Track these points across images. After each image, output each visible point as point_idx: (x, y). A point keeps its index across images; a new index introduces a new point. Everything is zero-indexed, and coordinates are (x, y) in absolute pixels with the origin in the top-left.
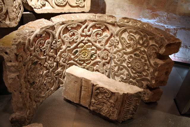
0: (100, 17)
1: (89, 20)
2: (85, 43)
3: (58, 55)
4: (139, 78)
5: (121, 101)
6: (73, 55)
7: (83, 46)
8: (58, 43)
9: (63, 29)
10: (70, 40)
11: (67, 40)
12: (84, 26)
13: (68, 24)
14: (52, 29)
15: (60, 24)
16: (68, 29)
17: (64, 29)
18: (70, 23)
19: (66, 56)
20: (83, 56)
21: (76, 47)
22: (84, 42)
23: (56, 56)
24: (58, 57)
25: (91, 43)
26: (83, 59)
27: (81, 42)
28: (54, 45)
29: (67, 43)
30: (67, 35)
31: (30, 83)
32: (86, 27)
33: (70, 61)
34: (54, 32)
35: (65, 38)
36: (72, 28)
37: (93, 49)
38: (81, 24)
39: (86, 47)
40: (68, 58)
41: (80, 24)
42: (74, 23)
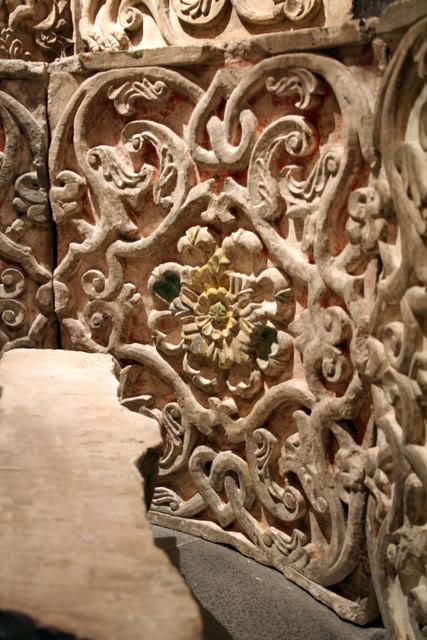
0: (315, 225)
1: (234, 53)
2: (218, 230)
3: (56, 271)
4: (42, 44)
5: (251, 174)
6: (158, 309)
7: (206, 249)
8: (55, 189)
9: (85, 102)
10: (127, 191)
11: (110, 185)
12: (204, 99)
13: (110, 76)
14: (24, 97)
15: (73, 74)
16: (116, 113)
17: (90, 106)
18: (120, 73)
19: (104, 294)
20: (209, 330)
21: (166, 248)
22: (209, 214)
23: (42, 269)
24: (56, 282)
25: (258, 234)
26: (209, 349)
27: (191, 215)
28: (30, 194)
29: (113, 204)
30: (120, 153)
31: (376, 289)
32: (217, 108)
33: (135, 347)
34: (35, 119)
35: (101, 168)
36: (141, 107)
37: (261, 290)
38: (189, 83)
39: (224, 260)
40: (121, 316)
41: (180, 78)
42: (146, 70)
